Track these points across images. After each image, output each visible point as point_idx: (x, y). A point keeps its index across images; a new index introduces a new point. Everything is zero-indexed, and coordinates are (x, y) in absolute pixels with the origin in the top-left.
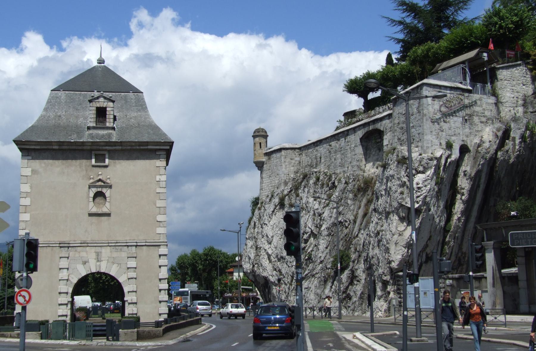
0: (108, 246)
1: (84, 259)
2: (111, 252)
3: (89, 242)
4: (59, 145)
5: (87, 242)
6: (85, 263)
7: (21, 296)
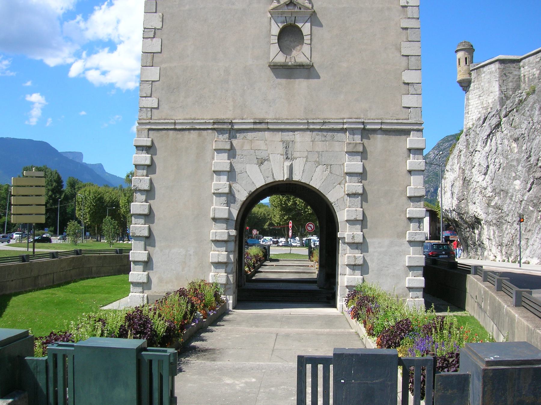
0: (307, 130)
1: (264, 155)
2: (313, 141)
3: (269, 121)
5: (267, 121)
6: (261, 162)
7: (309, 226)
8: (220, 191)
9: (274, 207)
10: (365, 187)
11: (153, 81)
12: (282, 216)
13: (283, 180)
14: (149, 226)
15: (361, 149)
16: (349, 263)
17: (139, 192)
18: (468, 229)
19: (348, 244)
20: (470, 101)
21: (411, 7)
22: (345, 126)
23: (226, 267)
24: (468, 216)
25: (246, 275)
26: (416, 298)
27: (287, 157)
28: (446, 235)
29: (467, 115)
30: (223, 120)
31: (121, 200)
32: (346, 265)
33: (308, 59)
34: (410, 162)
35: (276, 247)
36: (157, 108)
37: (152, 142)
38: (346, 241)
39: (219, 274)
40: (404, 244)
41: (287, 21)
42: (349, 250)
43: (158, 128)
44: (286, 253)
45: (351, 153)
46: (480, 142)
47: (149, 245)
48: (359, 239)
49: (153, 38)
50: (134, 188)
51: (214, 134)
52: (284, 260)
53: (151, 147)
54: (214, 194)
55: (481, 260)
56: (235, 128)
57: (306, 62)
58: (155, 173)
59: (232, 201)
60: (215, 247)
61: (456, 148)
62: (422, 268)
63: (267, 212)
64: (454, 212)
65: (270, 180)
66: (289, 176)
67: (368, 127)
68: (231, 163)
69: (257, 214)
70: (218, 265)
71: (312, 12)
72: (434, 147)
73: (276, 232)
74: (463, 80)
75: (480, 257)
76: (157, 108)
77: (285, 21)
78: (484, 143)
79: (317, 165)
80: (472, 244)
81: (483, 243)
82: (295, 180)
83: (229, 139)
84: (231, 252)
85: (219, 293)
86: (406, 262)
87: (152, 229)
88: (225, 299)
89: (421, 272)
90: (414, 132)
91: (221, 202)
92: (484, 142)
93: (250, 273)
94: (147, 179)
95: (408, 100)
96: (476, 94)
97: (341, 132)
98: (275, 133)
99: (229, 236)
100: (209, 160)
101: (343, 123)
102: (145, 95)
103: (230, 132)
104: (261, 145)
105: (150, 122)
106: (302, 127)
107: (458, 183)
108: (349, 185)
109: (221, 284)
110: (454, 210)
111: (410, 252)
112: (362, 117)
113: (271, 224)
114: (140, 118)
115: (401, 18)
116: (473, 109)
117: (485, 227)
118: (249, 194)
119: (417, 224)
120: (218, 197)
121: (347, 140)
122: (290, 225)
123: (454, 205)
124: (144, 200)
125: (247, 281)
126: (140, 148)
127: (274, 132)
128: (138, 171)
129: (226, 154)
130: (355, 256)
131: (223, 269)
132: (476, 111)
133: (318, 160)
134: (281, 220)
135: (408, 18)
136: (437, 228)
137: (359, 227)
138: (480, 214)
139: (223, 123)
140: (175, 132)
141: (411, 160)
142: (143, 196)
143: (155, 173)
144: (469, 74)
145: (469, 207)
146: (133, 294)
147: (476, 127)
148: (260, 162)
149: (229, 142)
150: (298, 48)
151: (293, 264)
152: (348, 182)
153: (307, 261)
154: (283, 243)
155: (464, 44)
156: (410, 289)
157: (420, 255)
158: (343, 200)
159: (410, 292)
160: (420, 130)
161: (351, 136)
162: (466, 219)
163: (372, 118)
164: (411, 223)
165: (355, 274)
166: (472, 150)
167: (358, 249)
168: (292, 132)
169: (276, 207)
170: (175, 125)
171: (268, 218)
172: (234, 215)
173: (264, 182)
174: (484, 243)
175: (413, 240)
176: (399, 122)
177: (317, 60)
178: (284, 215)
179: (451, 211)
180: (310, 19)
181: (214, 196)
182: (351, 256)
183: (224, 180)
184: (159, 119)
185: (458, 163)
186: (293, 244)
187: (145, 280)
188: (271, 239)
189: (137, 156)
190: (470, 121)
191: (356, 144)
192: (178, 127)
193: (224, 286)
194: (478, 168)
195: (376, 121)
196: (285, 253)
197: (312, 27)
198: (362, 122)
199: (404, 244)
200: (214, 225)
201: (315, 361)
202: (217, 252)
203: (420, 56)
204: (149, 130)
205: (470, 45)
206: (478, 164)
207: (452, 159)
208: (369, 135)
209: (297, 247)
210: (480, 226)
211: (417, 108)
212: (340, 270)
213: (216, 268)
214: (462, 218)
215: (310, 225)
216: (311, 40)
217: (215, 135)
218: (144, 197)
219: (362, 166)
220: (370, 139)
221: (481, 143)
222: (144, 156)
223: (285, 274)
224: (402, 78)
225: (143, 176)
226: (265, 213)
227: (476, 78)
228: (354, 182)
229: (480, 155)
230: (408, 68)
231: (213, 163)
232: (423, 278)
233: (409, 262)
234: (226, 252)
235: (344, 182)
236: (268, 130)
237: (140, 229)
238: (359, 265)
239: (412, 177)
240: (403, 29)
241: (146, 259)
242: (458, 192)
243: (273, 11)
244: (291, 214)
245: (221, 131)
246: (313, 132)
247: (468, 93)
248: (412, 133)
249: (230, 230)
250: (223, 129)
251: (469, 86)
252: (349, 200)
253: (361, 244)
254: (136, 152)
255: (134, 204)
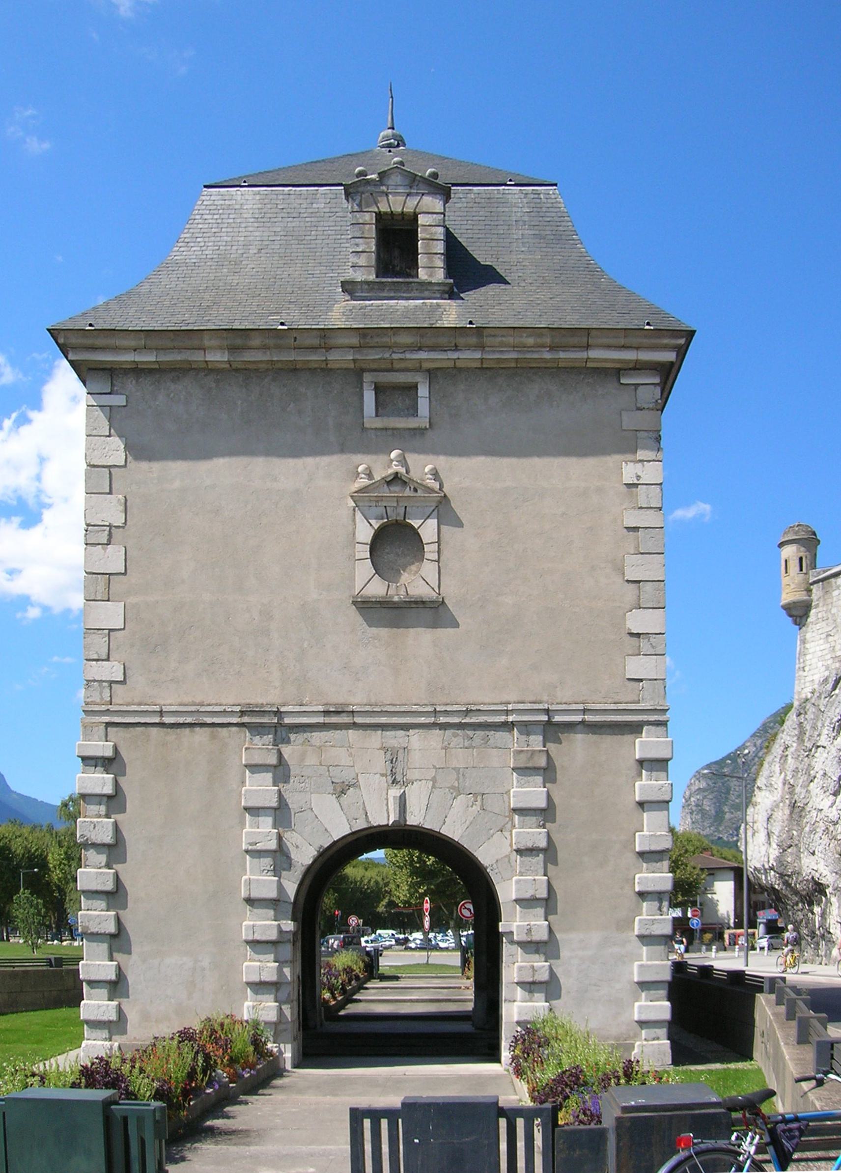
0: (435, 725)
1: (347, 776)
2: (446, 748)
4: (233, 349)
5: (351, 708)
6: (341, 790)
7: (465, 908)
8: (259, 847)
9: (397, 869)
10: (551, 835)
11: (110, 630)
12: (413, 886)
13: (388, 825)
14: (117, 913)
15: (542, 762)
16: (522, 980)
17: (92, 848)
18: (800, 905)
19: (520, 944)
20: (807, 646)
21: (645, 486)
22: (511, 719)
23: (277, 990)
24: (800, 879)
25: (324, 1007)
26: (654, 1039)
27: (395, 779)
28: (770, 918)
29: (801, 673)
30: (262, 707)
31: (50, 855)
32: (517, 983)
33: (433, 589)
34: (641, 785)
35: (401, 951)
36: (123, 682)
37: (116, 749)
38: (515, 938)
39: (263, 1004)
40: (630, 941)
41: (389, 514)
42: (522, 955)
43: (127, 721)
44: (419, 964)
45: (523, 771)
46: (827, 728)
47: (119, 951)
48: (543, 935)
49: (107, 544)
50: (82, 840)
51: (243, 735)
52: (409, 977)
53: (114, 759)
54: (247, 851)
55: (826, 964)
56: (286, 722)
57: (430, 596)
58: (124, 812)
59: (285, 866)
60: (252, 953)
61: (778, 741)
62: (667, 985)
63: (383, 879)
64: (772, 873)
65: (360, 825)
66: (400, 817)
67: (557, 718)
68: (279, 791)
69: (361, 884)
70: (259, 987)
71: (441, 497)
72: (756, 732)
73: (403, 919)
74: (794, 603)
75: (824, 959)
76: (121, 681)
77: (385, 516)
78: (833, 730)
79: (454, 794)
80: (807, 936)
81: (829, 933)
82: (411, 824)
83: (273, 745)
84: (287, 962)
85: (263, 1040)
86: (633, 975)
87: (123, 920)
88: (275, 1050)
89: (663, 993)
90: (650, 727)
91: (262, 869)
92: (834, 728)
93: (333, 1003)
94: (108, 823)
95: (637, 667)
96: (820, 632)
97: (502, 729)
98: (368, 732)
99: (281, 931)
100: (235, 786)
101: (507, 712)
102: (96, 657)
103: (276, 731)
104: (341, 756)
105: (108, 710)
106: (422, 720)
107: (780, 813)
108: (520, 832)
109: (266, 1023)
110: (772, 869)
111: (642, 955)
112: (545, 698)
113: (392, 904)
114: (89, 700)
115: (625, 509)
116: (814, 661)
117: (834, 899)
118: (318, 851)
119: (656, 904)
120: (257, 858)
121: (515, 745)
122: (427, 906)
123: (772, 857)
124: (103, 864)
125: (326, 1020)
126: (89, 761)
127: (366, 730)
128: (89, 806)
129: (270, 775)
130: (533, 967)
131: (270, 994)
132: (820, 664)
133: (456, 784)
134: (411, 895)
135: (639, 508)
136: (752, 902)
137: (540, 911)
138: (823, 875)
139: (262, 713)
140: (161, 729)
141: (644, 782)
142: (101, 856)
143: (124, 812)
144: (806, 590)
145: (803, 862)
146: (90, 1042)
147: (819, 697)
148: (339, 789)
149: (275, 751)
150: (413, 568)
151: (428, 983)
152: (517, 826)
153: (458, 977)
154: (418, 942)
155: (797, 529)
156: (643, 1024)
157: (662, 960)
158: (509, 861)
159: (642, 1029)
160: (664, 724)
161: (524, 738)
162: (795, 885)
163: (564, 701)
164: (643, 902)
165: (534, 999)
166: (809, 745)
167: (538, 953)
168: (402, 729)
169: (401, 868)
170: (162, 716)
171: (386, 892)
172: (289, 893)
173: (349, 829)
174: (831, 931)
175: (647, 933)
176: (619, 708)
177: (451, 592)
178: (419, 884)
179: (765, 870)
180: (436, 510)
181: (248, 857)
182: (526, 967)
183: (266, 824)
184: (128, 705)
185: (781, 773)
186: (442, 945)
187: (113, 1017)
188: (393, 935)
189: (84, 777)
190: (807, 684)
191: (533, 752)
192: (167, 720)
193: (273, 1026)
194: (821, 782)
195: (574, 707)
196: (415, 963)
197: (442, 526)
198: (544, 709)
199: (630, 941)
200: (248, 912)
201: (375, 1115)
202: (258, 964)
203: (663, 581)
204: (108, 724)
205: (810, 531)
206: (821, 773)
207: (768, 763)
208: (560, 734)
209: (450, 951)
210: (824, 899)
211: (656, 680)
212: (505, 993)
213: (256, 992)
214: (787, 884)
215: (467, 906)
216: (439, 552)
217: (245, 737)
218: (103, 858)
219: (544, 796)
220: (561, 743)
221: (828, 730)
222: (98, 778)
223: (409, 1004)
224: (625, 624)
225: (100, 816)
226: (379, 879)
227: (822, 600)
228: (529, 826)
229: (825, 755)
230: (639, 605)
231: (243, 792)
232: (668, 1004)
233: (639, 974)
234: (276, 962)
235: (509, 825)
236: (355, 726)
237: (97, 920)
238: (541, 983)
239: (645, 814)
240: (629, 529)
241: (113, 977)
242: (779, 832)
243: (360, 494)
244: (434, 883)
245: (257, 729)
246: (445, 730)
247: (804, 628)
248: (645, 728)
249: (282, 922)
250: (261, 725)
251: (806, 615)
252: (520, 861)
253: (545, 943)
254: (83, 769)
255: (84, 872)
